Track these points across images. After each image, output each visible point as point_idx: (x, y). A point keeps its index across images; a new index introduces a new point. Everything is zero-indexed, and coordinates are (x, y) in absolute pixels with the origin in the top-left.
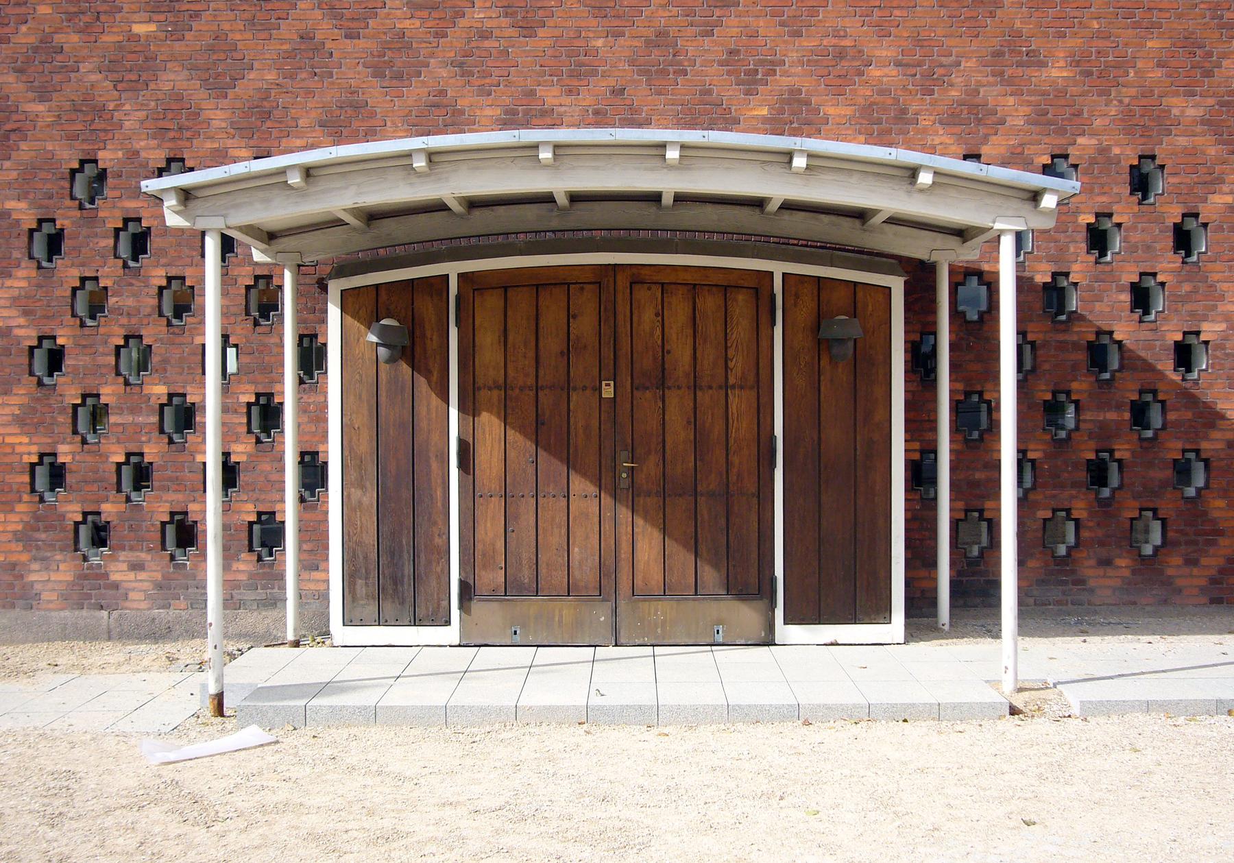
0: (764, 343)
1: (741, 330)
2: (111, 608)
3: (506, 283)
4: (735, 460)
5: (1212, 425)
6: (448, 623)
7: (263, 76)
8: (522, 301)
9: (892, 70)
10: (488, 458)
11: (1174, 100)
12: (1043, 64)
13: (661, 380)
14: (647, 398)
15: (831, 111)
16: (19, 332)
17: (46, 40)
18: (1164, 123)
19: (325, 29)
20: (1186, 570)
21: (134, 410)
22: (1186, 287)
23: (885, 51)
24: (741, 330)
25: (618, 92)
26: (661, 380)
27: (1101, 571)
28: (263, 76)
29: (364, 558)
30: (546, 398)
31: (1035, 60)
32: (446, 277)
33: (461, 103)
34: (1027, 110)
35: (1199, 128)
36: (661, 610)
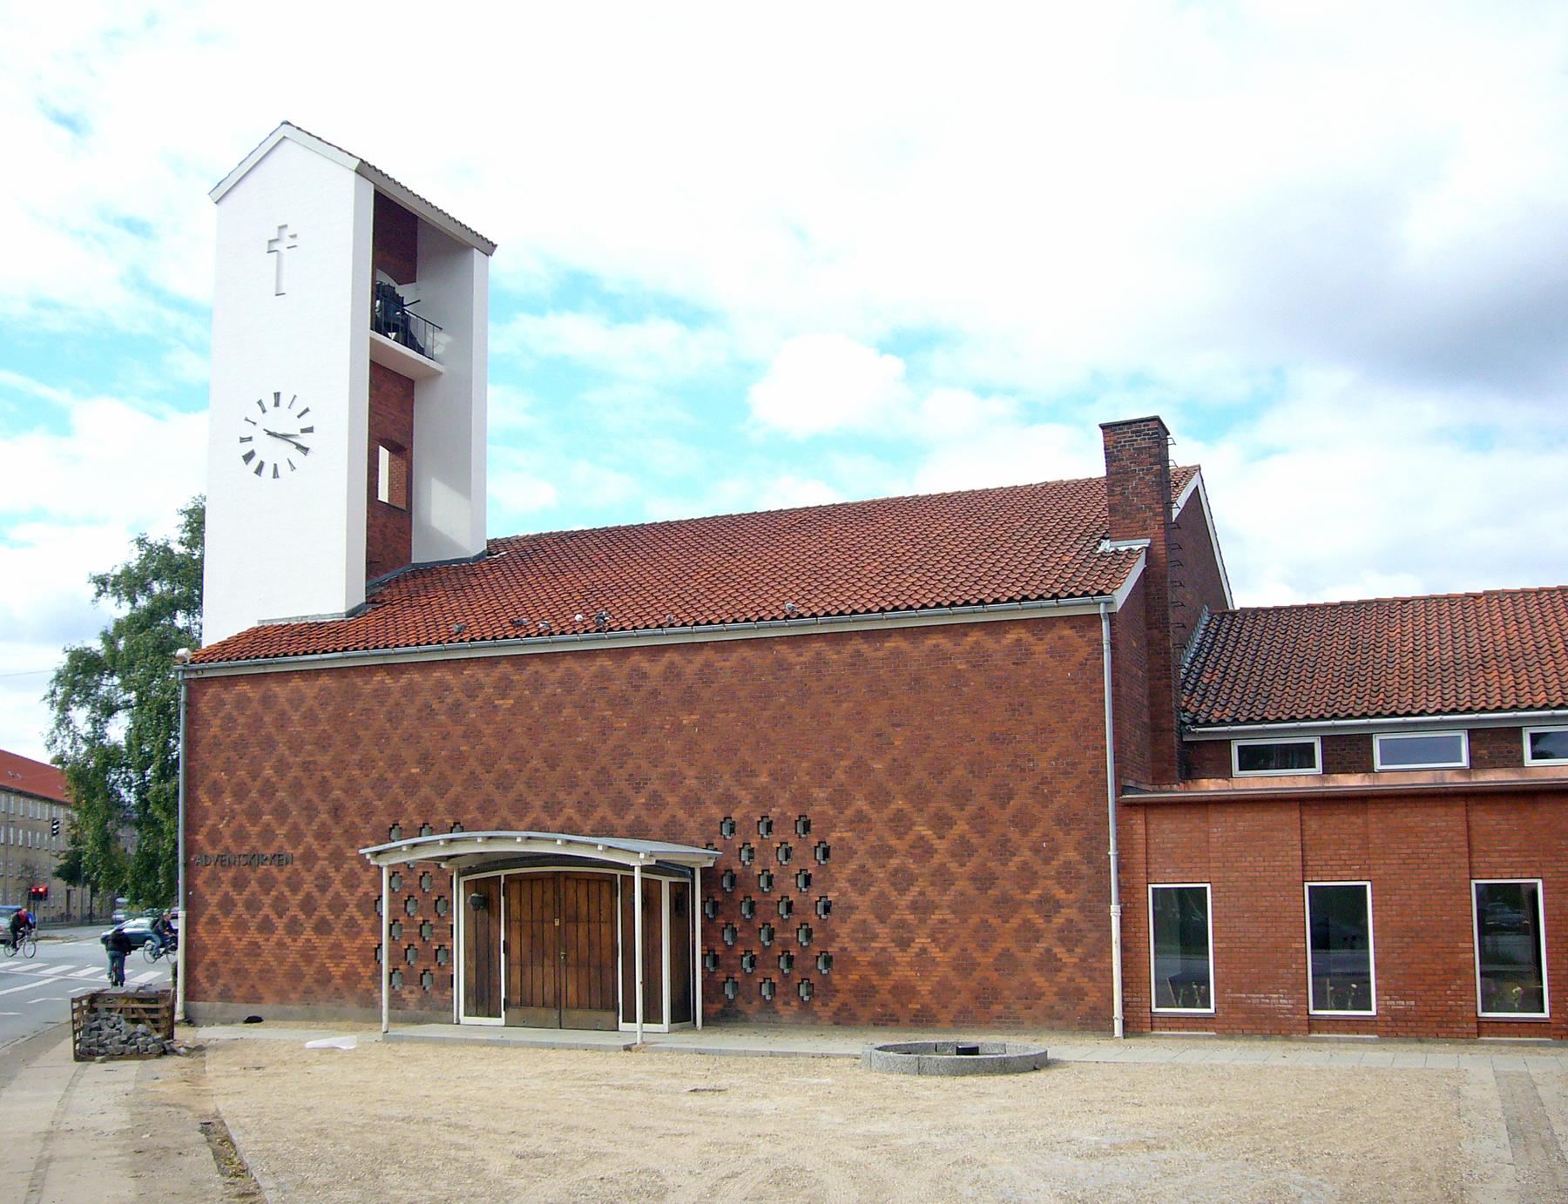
0: (614, 903)
1: (606, 896)
2: (403, 1009)
3: (521, 879)
4: (603, 952)
5: (833, 940)
6: (500, 1016)
7: (457, 789)
8: (526, 885)
9: (694, 781)
10: (515, 949)
11: (813, 790)
12: (757, 776)
13: (576, 919)
14: (571, 927)
15: (670, 799)
16: (372, 894)
17: (381, 775)
18: (810, 801)
19: (479, 770)
20: (822, 1008)
21: (411, 927)
22: (820, 876)
23: (691, 773)
24: (606, 896)
25: (587, 794)
26: (576, 919)
27: (785, 1007)
28: (457, 789)
29: (1201, 1104)
30: (535, 926)
31: (753, 774)
32: (500, 876)
33: (529, 799)
34: (750, 796)
35: (825, 803)
36: (577, 1014)
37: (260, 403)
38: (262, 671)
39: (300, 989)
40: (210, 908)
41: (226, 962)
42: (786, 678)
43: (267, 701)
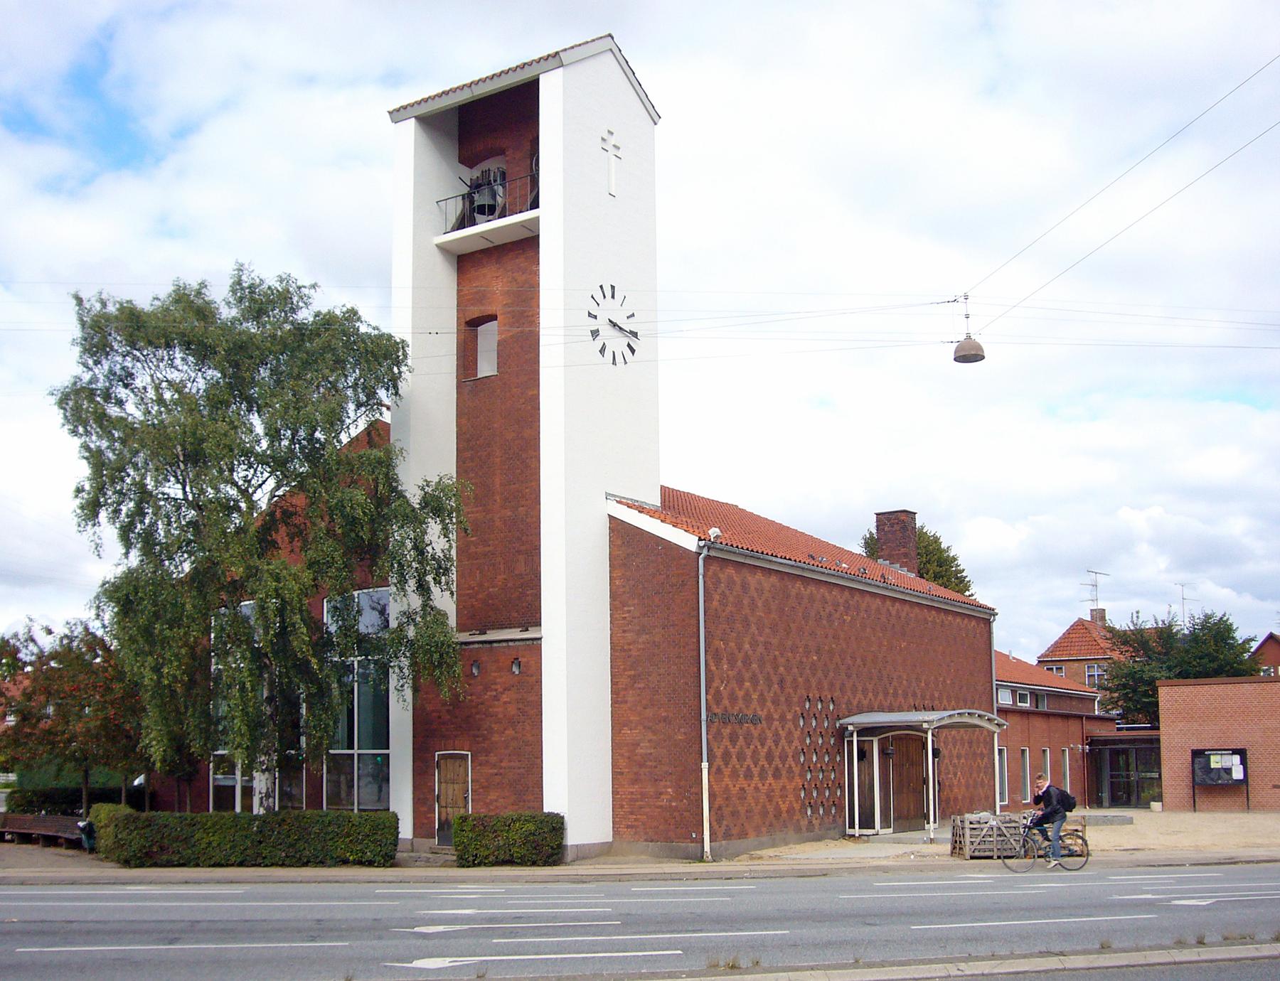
37: (601, 287)
38: (743, 561)
39: (767, 823)
40: (717, 760)
41: (727, 806)
42: (111, 666)
43: (745, 587)
